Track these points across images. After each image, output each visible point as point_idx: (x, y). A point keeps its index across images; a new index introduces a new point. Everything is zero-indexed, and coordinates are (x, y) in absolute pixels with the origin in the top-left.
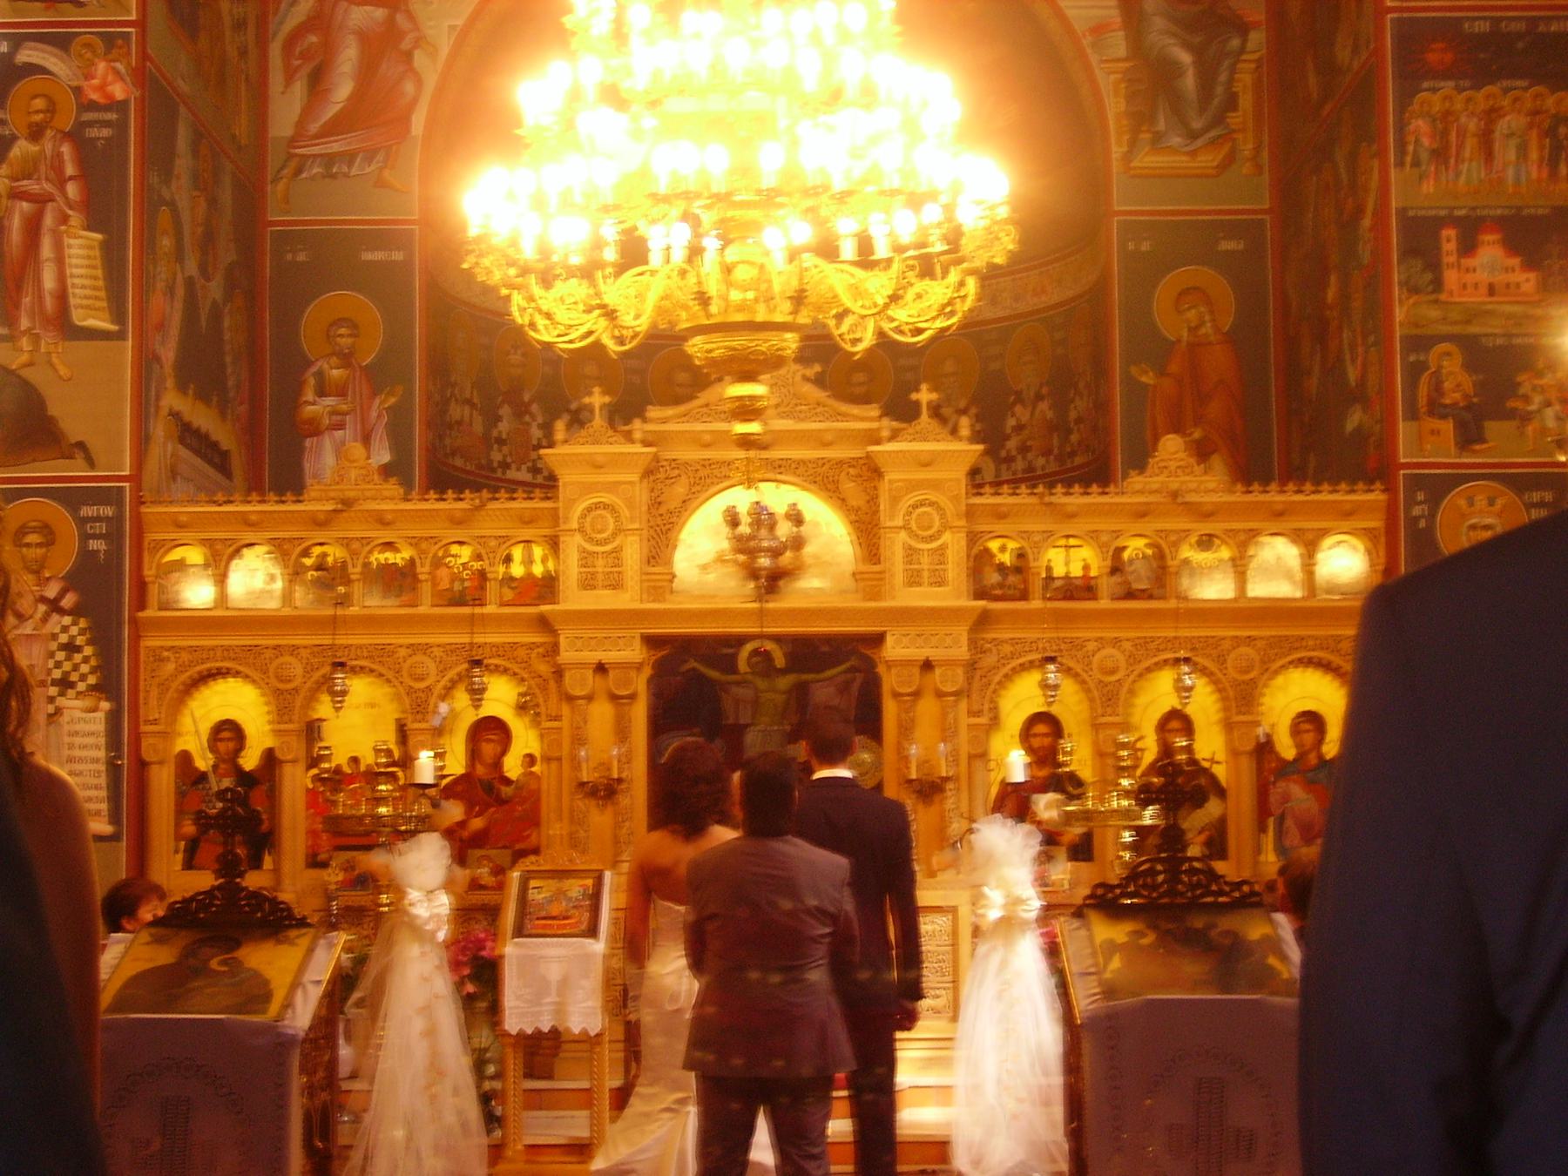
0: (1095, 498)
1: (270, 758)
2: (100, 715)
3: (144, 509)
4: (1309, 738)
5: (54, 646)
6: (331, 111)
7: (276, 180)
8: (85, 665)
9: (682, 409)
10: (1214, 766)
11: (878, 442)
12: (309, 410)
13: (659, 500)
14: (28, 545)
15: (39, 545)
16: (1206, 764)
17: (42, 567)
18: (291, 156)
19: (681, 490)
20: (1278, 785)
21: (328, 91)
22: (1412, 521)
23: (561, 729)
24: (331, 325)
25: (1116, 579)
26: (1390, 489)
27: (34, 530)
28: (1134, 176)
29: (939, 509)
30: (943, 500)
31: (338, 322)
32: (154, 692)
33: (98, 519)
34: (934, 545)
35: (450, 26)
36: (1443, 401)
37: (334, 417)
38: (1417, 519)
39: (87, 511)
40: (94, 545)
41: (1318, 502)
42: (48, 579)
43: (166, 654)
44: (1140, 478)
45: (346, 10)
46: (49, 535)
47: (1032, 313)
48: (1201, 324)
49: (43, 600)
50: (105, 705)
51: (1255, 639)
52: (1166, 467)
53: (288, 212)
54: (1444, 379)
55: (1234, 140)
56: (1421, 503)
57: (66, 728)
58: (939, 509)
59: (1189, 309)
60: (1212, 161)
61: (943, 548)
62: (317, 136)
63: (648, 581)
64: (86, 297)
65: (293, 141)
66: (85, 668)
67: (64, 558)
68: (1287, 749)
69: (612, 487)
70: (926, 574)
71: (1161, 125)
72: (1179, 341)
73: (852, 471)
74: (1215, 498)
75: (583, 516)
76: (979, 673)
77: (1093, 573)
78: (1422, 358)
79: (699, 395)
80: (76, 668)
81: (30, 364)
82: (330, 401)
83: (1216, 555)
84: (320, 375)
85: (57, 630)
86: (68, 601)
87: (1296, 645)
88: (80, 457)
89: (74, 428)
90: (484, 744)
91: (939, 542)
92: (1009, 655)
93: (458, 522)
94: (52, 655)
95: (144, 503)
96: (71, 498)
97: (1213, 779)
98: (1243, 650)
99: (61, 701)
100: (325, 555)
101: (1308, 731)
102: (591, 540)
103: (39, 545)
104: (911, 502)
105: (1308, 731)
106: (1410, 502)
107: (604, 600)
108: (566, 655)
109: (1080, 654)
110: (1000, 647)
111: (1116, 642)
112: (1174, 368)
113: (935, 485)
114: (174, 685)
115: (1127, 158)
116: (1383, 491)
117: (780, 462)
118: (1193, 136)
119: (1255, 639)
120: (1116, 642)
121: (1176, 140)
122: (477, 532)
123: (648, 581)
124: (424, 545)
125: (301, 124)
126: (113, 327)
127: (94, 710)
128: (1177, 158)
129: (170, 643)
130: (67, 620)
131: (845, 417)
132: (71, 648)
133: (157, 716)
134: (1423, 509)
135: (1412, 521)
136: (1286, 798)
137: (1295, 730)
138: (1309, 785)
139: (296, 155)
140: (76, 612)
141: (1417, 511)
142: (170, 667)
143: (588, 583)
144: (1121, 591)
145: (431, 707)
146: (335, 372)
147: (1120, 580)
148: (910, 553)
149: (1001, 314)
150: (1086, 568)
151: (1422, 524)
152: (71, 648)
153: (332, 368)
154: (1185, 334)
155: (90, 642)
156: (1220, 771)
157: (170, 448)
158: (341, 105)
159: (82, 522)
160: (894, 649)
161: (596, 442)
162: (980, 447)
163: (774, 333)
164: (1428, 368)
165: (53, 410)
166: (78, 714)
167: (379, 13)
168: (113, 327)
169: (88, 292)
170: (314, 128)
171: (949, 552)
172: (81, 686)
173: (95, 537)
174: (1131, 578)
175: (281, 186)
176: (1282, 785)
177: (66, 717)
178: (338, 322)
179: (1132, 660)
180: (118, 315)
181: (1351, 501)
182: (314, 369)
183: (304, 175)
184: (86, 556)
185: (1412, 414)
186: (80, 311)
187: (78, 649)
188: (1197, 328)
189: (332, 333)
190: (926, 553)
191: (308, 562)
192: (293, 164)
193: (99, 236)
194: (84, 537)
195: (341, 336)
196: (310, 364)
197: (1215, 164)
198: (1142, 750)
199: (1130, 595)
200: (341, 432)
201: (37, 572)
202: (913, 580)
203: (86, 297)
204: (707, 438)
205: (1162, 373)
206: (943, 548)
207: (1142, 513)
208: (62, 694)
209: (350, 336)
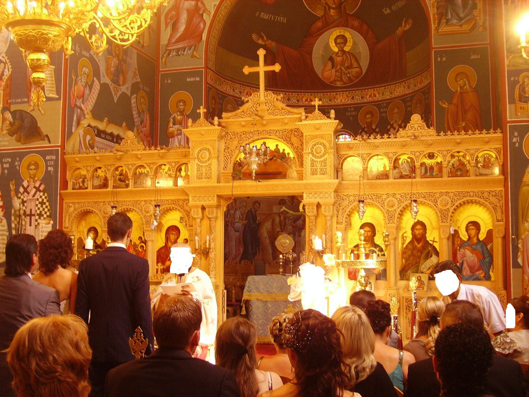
0: (386, 140)
1: (490, 233)
2: (50, 225)
3: (65, 156)
4: (473, 232)
5: (37, 202)
6: (178, 35)
7: (162, 58)
8: (46, 210)
9: (234, 113)
10: (434, 243)
11: (301, 121)
12: (171, 130)
13: (228, 146)
14: (31, 169)
15: (34, 169)
16: (431, 242)
17: (35, 176)
18: (167, 50)
19: (236, 143)
20: (461, 250)
21: (178, 28)
22: (513, 144)
23: (192, 229)
24: (177, 102)
25: (396, 171)
26: (503, 132)
27: (33, 164)
28: (440, 35)
29: (324, 145)
30: (325, 142)
31: (179, 101)
32: (67, 218)
33: (51, 160)
34: (322, 159)
35: (214, 5)
36: (525, 95)
37: (178, 131)
38: (515, 143)
39: (48, 158)
40: (49, 169)
41: (474, 138)
42: (37, 181)
43: (71, 205)
44: (404, 132)
45: (184, 3)
46: (37, 165)
47: (419, 90)
48: (465, 85)
49: (35, 187)
50: (52, 222)
51: (449, 193)
52: (413, 127)
53: (165, 68)
54: (526, 86)
55: (476, 20)
56: (516, 137)
57: (41, 230)
58: (324, 145)
59: (460, 80)
60: (468, 28)
61: (325, 160)
62: (175, 43)
63: (224, 176)
64: (50, 87)
65: (167, 46)
66: (46, 210)
67: (41, 174)
68: (464, 236)
69: (207, 142)
70: (319, 170)
71: (449, 16)
72: (457, 91)
73: (296, 133)
74: (433, 138)
75: (199, 153)
76: (341, 208)
77: (388, 169)
78: (516, 79)
79: (240, 108)
80: (44, 209)
81: (34, 110)
82: (177, 126)
83: (435, 161)
84: (174, 119)
85: (39, 197)
86: (42, 188)
87: (466, 195)
88: (46, 139)
89: (45, 130)
90: (171, 235)
91: (324, 158)
92: (353, 201)
93: (162, 157)
94: (37, 205)
95: (65, 154)
96: (43, 154)
97: (434, 248)
98: (444, 197)
99: (39, 221)
100: (122, 170)
101: (473, 229)
102: (201, 162)
103: (34, 169)
104: (314, 143)
105: (473, 229)
106: (512, 136)
107: (204, 183)
108: (191, 203)
109: (380, 200)
110: (349, 198)
111: (394, 195)
112: (455, 101)
113: (322, 137)
114: (73, 215)
115: (437, 29)
116: (501, 133)
117: (270, 131)
118: (461, 19)
119: (449, 193)
120: (394, 195)
121: (455, 21)
122: (169, 161)
123: (224, 176)
124: (151, 166)
125: (170, 40)
126: (57, 97)
127: (49, 223)
128: (457, 28)
129: (72, 201)
130: (42, 194)
131: (292, 113)
132: (42, 203)
133: (68, 226)
134: (517, 139)
135: (513, 144)
136: (464, 256)
137: (467, 229)
138: (473, 251)
139: (168, 49)
140: (44, 191)
141: (514, 140)
142: (72, 209)
143: (199, 178)
144: (398, 175)
145: (151, 222)
146: (179, 117)
147: (398, 171)
148: (313, 162)
149: (411, 91)
150: (385, 167)
151: (517, 145)
152: (42, 203)
153: (178, 116)
154: (459, 89)
155: (47, 201)
156: (436, 245)
157: (88, 138)
158: (181, 33)
159: (46, 161)
160: (306, 200)
161: (201, 126)
162: (337, 121)
163: (48, 27)
164: (519, 83)
165: (39, 125)
166: (44, 225)
167: (193, 3)
168: (57, 97)
169: (50, 85)
170: (173, 40)
171: (328, 162)
172: (45, 216)
173: (50, 166)
174: (402, 171)
175: (164, 60)
176: (462, 250)
177: (41, 225)
178: (179, 101)
179: (400, 202)
180: (58, 93)
181: (488, 137)
182: (173, 116)
183: (171, 55)
184: (47, 172)
185: (512, 101)
186: (48, 92)
187: (45, 204)
188: (464, 86)
189: (178, 105)
190: (319, 162)
191: (117, 173)
192: (167, 53)
193: (54, 67)
194: (47, 166)
195: (181, 105)
196: (171, 115)
197: (469, 29)
198: (406, 237)
199: (402, 177)
200: (179, 137)
201: (33, 178)
202: (314, 173)
203: (50, 87)
204: (244, 123)
205: (450, 103)
206: (325, 160)
207: (404, 145)
208: (40, 218)
209: (183, 105)
